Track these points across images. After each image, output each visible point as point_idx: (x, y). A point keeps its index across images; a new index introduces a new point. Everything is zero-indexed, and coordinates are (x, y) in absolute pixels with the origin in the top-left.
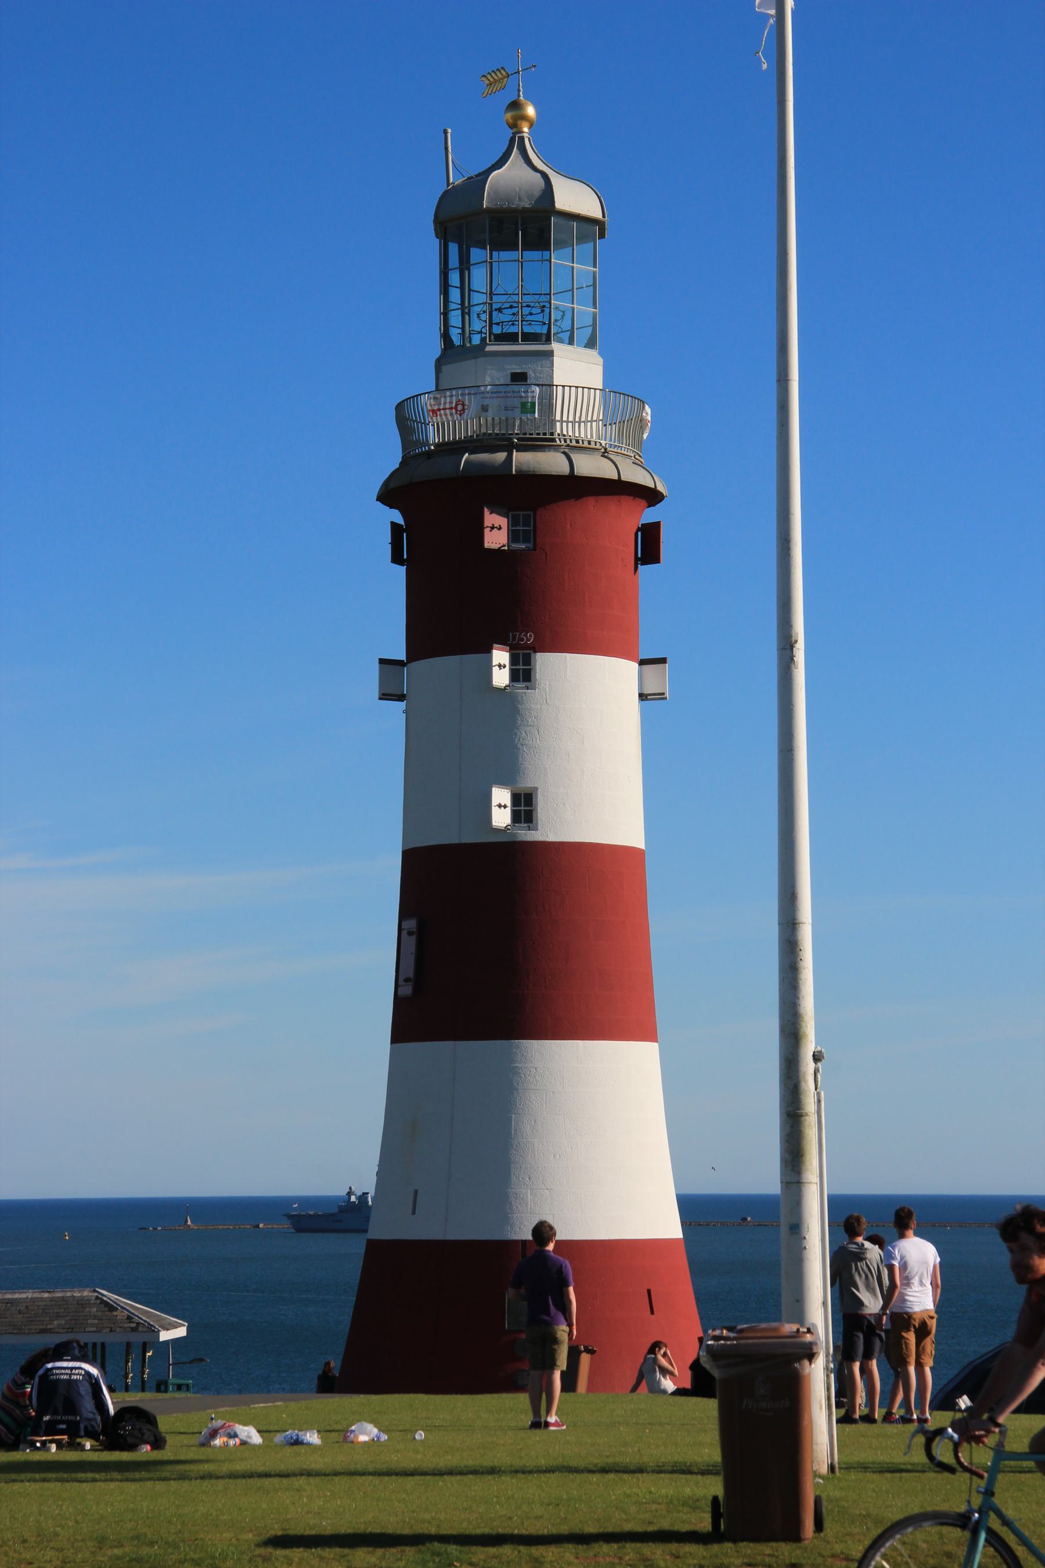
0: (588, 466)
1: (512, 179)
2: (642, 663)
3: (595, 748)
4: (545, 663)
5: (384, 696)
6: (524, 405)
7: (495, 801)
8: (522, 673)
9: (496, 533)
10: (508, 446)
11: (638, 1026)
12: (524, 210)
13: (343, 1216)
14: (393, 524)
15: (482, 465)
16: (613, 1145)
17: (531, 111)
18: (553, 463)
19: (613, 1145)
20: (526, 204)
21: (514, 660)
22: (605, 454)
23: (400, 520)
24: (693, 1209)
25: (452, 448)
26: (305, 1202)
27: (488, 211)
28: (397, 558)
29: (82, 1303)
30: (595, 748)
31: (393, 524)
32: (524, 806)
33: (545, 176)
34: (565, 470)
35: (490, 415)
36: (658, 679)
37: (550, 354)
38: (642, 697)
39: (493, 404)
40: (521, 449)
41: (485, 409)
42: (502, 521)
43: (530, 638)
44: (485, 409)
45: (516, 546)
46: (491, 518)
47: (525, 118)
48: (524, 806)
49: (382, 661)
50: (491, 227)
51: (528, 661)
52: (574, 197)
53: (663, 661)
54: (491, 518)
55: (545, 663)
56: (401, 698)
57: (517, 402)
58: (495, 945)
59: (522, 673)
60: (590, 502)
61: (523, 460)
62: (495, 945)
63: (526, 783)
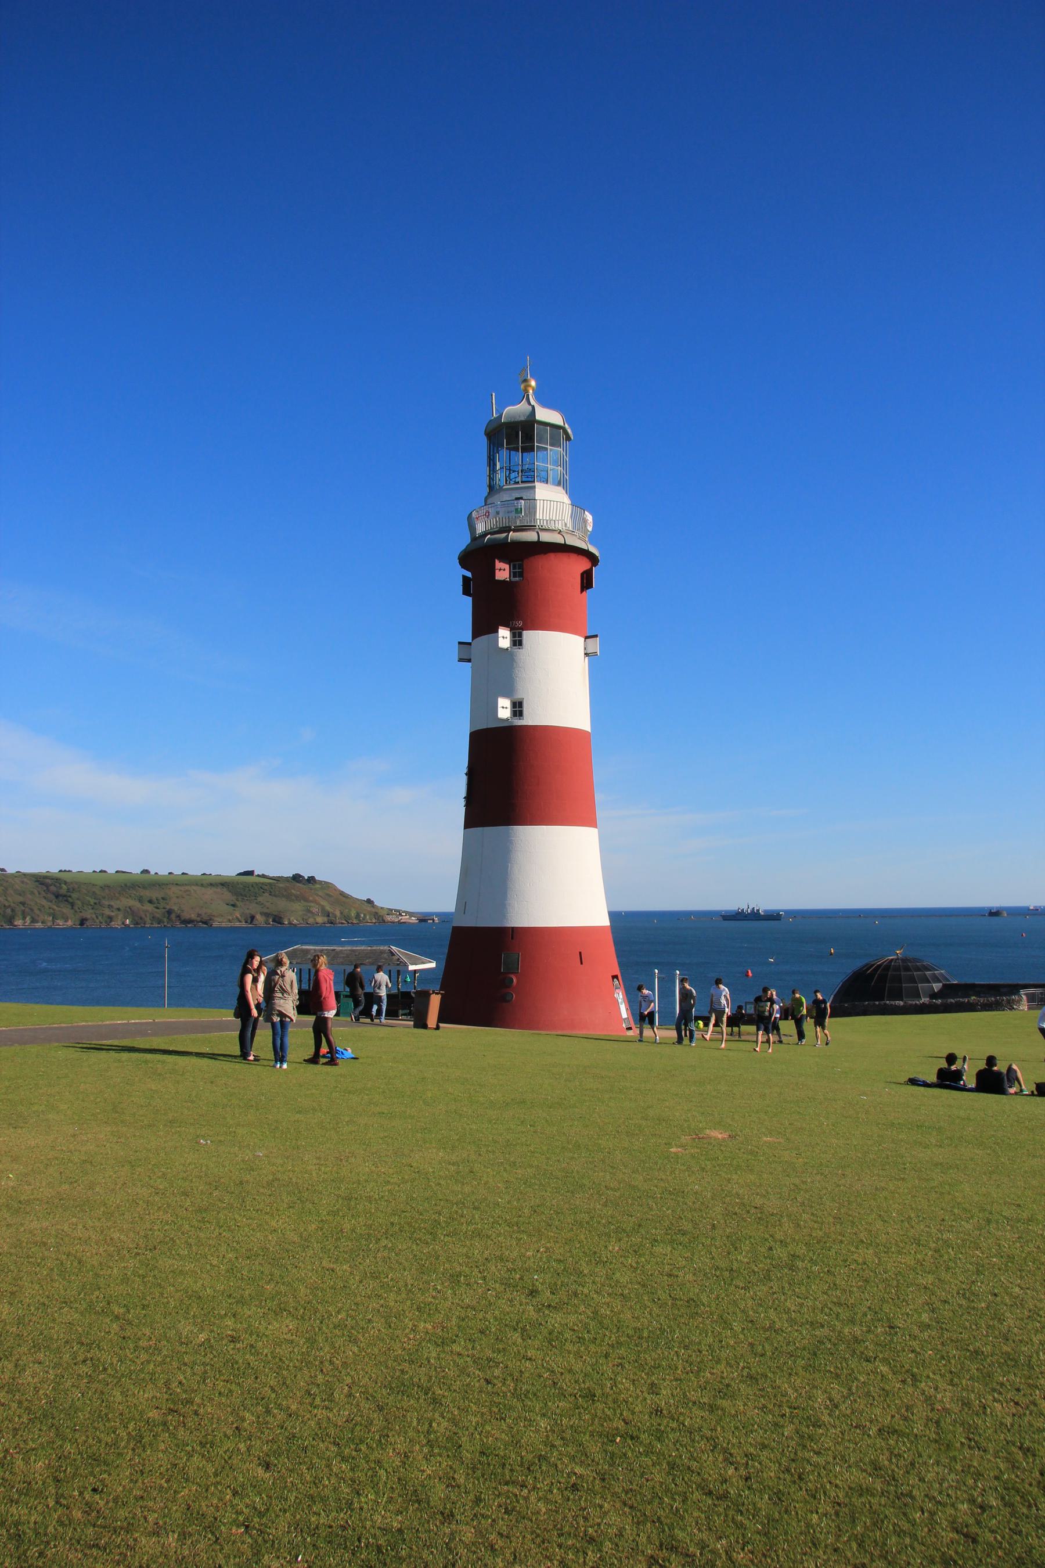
0: (546, 537)
1: (516, 410)
2: (586, 638)
3: (558, 679)
4: (527, 635)
5: (461, 660)
6: (516, 510)
7: (500, 705)
8: (517, 641)
9: (503, 572)
10: (507, 530)
11: (588, 819)
12: (522, 422)
13: (445, 917)
14: (464, 577)
15: (495, 539)
16: (566, 881)
17: (533, 383)
18: (530, 536)
19: (566, 881)
20: (523, 419)
21: (513, 635)
22: (560, 532)
23: (469, 574)
24: (613, 916)
25: (485, 535)
26: (726, 911)
27: (505, 423)
28: (466, 592)
29: (382, 952)
30: (558, 679)
31: (464, 577)
32: (518, 708)
33: (533, 407)
34: (536, 539)
35: (500, 516)
36: (595, 645)
37: (534, 487)
38: (586, 654)
39: (502, 511)
40: (515, 531)
41: (498, 513)
42: (507, 567)
43: (520, 624)
44: (498, 513)
45: (513, 579)
46: (499, 565)
47: (530, 386)
48: (518, 708)
49: (460, 643)
50: (517, 436)
51: (520, 635)
52: (544, 415)
53: (596, 636)
54: (499, 565)
55: (527, 635)
56: (469, 661)
57: (513, 509)
58: (509, 778)
59: (517, 641)
60: (552, 556)
61: (513, 536)
62: (509, 778)
63: (518, 696)
